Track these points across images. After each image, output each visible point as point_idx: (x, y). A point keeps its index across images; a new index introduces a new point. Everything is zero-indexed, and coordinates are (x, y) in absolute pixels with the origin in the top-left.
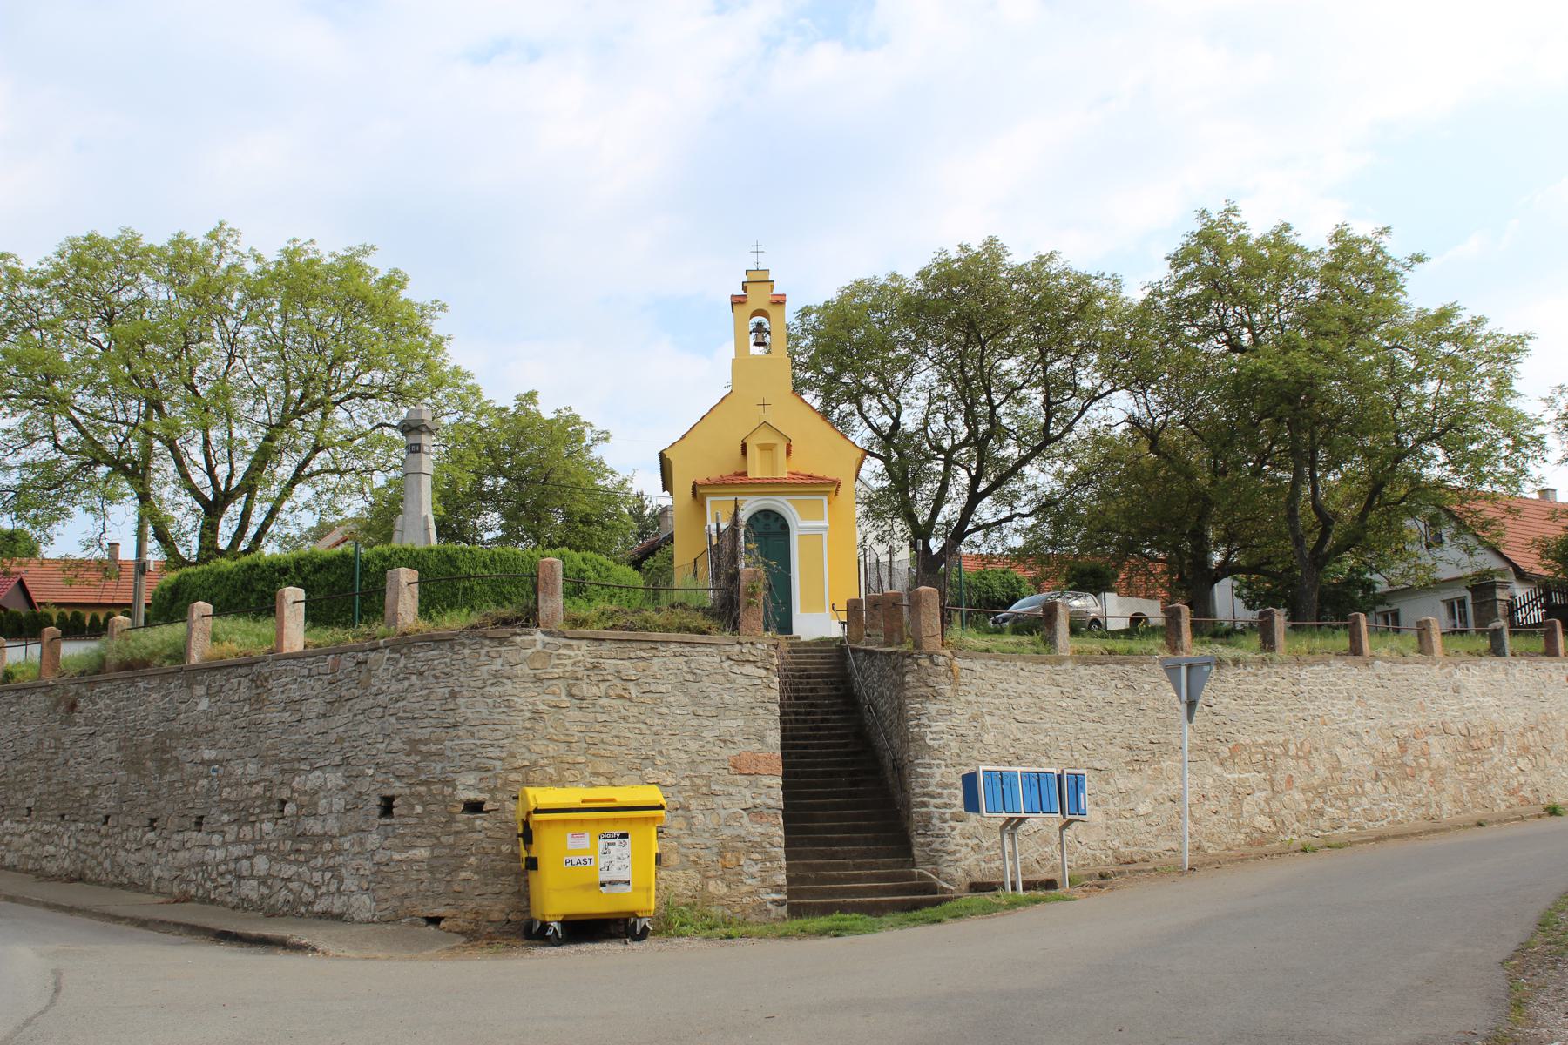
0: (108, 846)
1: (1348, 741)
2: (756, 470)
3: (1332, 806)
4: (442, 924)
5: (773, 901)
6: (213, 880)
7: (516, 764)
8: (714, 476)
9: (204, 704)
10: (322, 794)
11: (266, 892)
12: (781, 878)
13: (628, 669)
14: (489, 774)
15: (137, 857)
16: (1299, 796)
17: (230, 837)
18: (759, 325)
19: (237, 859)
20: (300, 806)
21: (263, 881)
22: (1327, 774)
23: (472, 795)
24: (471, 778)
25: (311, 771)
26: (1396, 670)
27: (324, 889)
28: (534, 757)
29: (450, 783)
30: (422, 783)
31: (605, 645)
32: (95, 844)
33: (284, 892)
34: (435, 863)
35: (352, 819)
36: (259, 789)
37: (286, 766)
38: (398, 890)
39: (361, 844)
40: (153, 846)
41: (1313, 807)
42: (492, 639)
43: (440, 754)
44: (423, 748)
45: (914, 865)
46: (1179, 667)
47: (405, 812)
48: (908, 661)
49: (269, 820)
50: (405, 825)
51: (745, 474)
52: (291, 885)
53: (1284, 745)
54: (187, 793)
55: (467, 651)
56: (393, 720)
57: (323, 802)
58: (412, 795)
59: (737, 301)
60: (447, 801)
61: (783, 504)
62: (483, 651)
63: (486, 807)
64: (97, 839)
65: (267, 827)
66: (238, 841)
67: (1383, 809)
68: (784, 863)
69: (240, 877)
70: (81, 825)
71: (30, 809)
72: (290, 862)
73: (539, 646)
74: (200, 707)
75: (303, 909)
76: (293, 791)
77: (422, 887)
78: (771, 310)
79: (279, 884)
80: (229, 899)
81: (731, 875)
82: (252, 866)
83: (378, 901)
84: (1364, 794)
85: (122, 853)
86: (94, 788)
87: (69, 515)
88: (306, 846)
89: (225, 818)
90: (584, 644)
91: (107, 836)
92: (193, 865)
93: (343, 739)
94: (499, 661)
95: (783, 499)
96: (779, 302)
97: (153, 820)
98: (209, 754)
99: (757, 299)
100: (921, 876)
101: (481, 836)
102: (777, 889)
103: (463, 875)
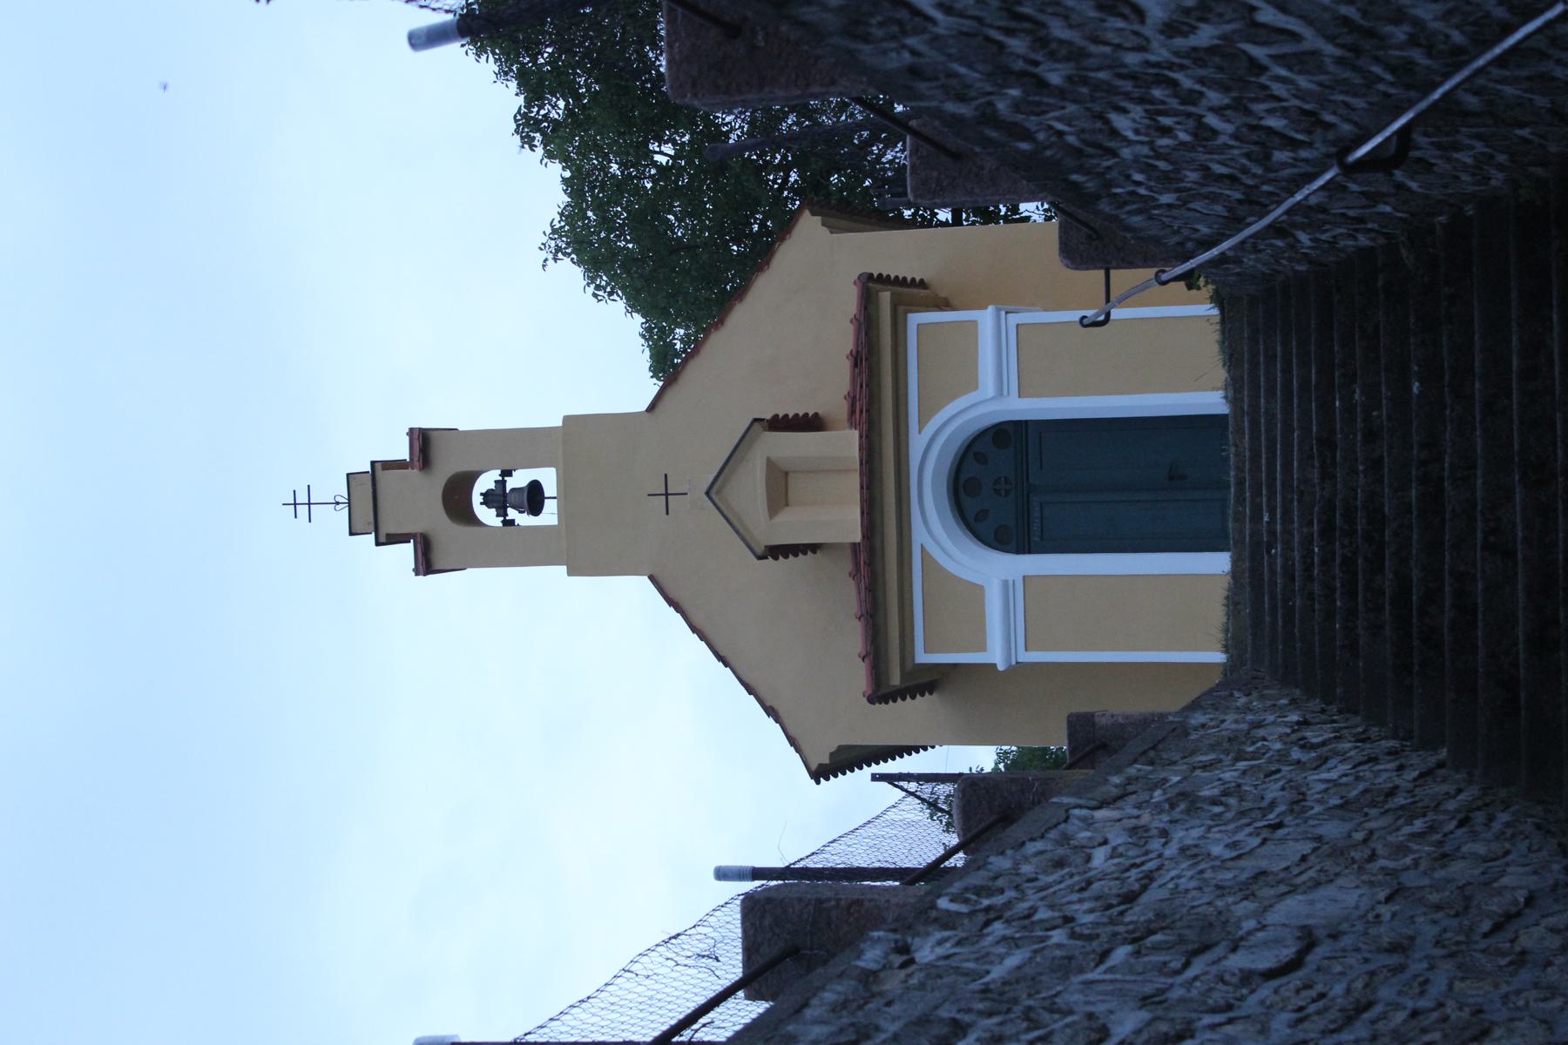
2: (842, 521)
8: (853, 638)
51: (854, 545)
61: (934, 437)
78: (447, 466)
87: (532, 147)
95: (917, 442)
99: (420, 502)
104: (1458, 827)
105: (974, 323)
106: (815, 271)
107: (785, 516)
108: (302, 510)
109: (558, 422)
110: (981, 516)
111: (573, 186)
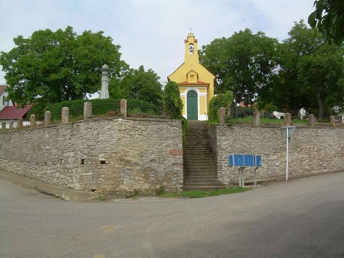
0: (29, 169)
1: (329, 147)
3: (325, 163)
4: (95, 191)
5: (180, 187)
6: (48, 178)
7: (114, 152)
9: (47, 136)
10: (69, 158)
11: (58, 181)
12: (182, 181)
13: (143, 127)
14: (107, 154)
15: (34, 171)
16: (317, 161)
17: (51, 168)
18: (191, 47)
19: (53, 173)
20: (65, 161)
21: (58, 178)
22: (324, 155)
23: (103, 159)
24: (102, 155)
25: (67, 152)
26: (341, 130)
27: (69, 181)
28: (118, 150)
29: (97, 156)
30: (91, 156)
31: (137, 122)
32: (27, 168)
33: (62, 181)
34: (94, 176)
35: (76, 164)
36: (57, 156)
37: (62, 151)
38: (85, 183)
39: (77, 171)
40: (37, 169)
41: (320, 163)
42: (108, 120)
43: (95, 149)
44: (91, 147)
45: (218, 178)
46: (286, 128)
47: (86, 163)
48: (218, 126)
49: (59, 164)
50: (87, 167)
52: (63, 180)
53: (314, 148)
54: (43, 157)
55: (102, 123)
56: (84, 140)
57: (69, 160)
58: (88, 159)
59: (186, 41)
60: (96, 161)
62: (106, 123)
63: (106, 163)
64: (27, 167)
65: (58, 165)
66: (53, 169)
67: (337, 164)
68: (182, 178)
69: (53, 177)
70: (24, 163)
71: (16, 159)
72: (63, 174)
73: (120, 122)
74: (46, 136)
75: (65, 186)
76: (64, 157)
77: (90, 182)
79: (61, 180)
80: (51, 182)
81: (169, 180)
82: (56, 175)
83: (81, 185)
84: (333, 160)
85: (32, 170)
86: (27, 155)
88: (66, 171)
89: (51, 163)
90: (131, 121)
91: (29, 166)
92: (44, 174)
93: (74, 145)
94: (110, 125)
95: (196, 88)
96: (196, 41)
97: (37, 163)
98: (48, 147)
99: (191, 40)
100: (219, 181)
101: (105, 170)
102: (181, 184)
103: (100, 179)
104: (142, 191)
105: (205, 92)
106: (208, 78)
107: (190, 76)
108: (190, 29)
109: (17, 37)
110: (190, 93)
111: (82, 35)
